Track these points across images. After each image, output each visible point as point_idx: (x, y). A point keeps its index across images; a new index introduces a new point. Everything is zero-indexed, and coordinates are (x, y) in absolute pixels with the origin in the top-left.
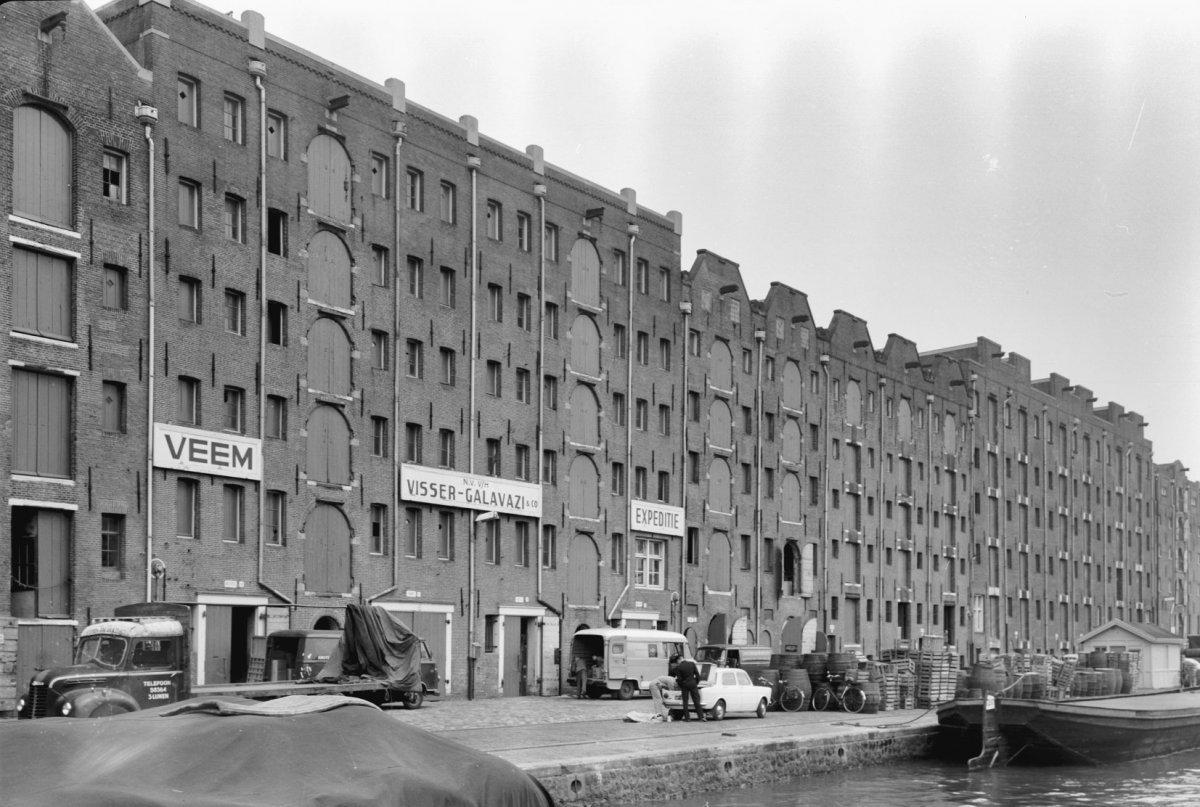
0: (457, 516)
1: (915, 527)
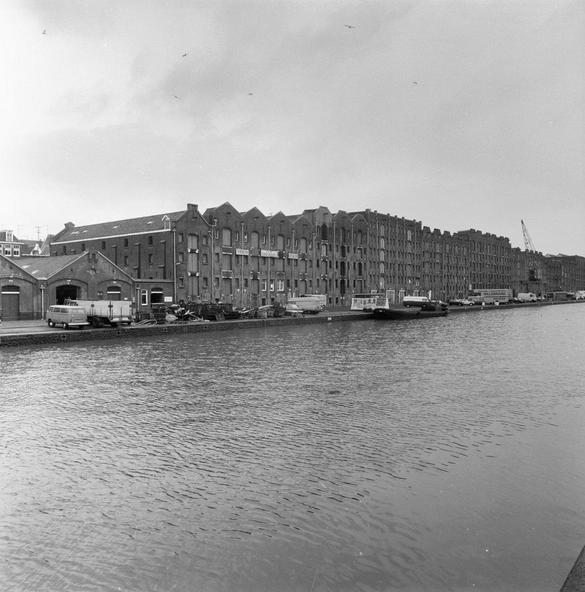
0: (239, 257)
1: (450, 270)
